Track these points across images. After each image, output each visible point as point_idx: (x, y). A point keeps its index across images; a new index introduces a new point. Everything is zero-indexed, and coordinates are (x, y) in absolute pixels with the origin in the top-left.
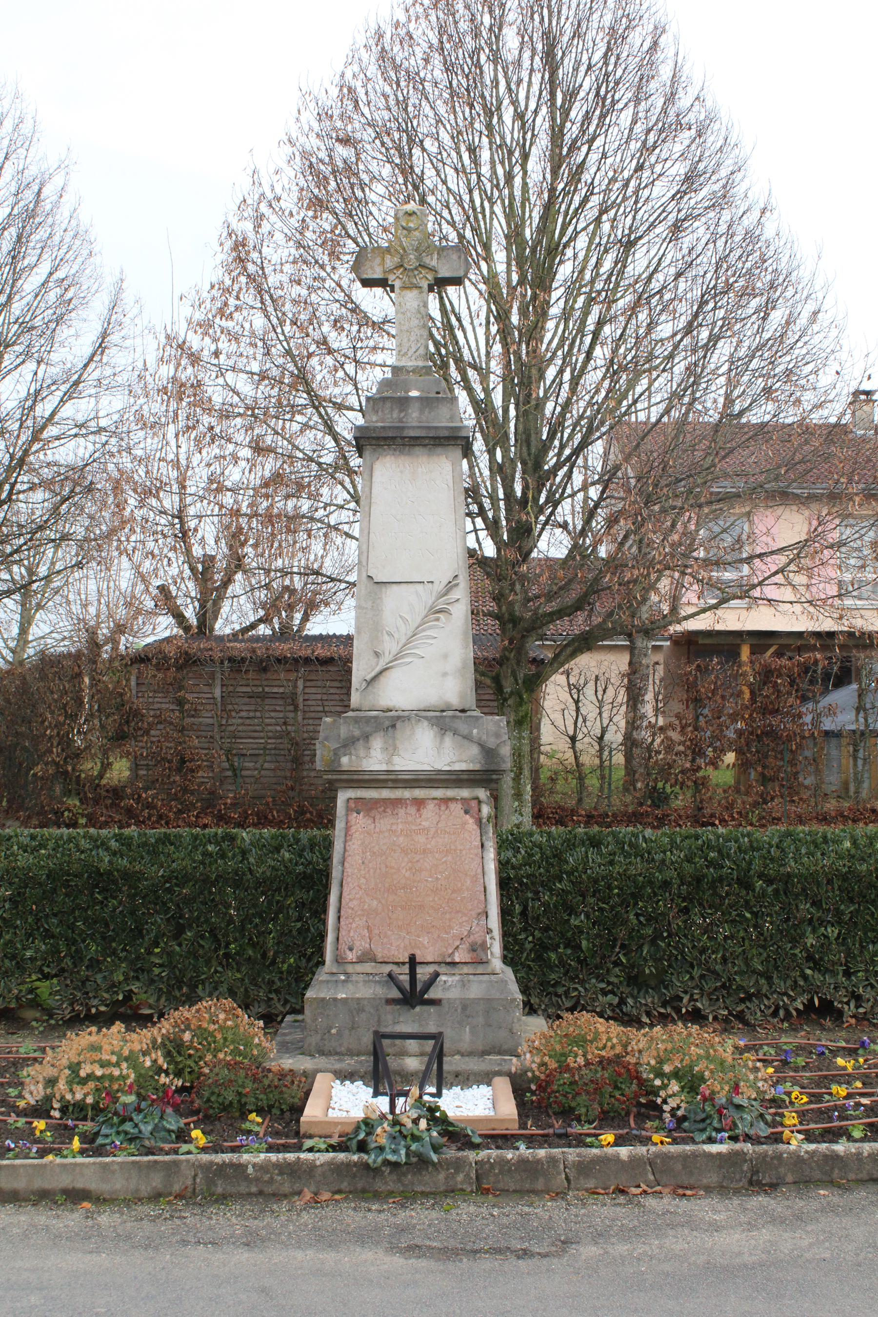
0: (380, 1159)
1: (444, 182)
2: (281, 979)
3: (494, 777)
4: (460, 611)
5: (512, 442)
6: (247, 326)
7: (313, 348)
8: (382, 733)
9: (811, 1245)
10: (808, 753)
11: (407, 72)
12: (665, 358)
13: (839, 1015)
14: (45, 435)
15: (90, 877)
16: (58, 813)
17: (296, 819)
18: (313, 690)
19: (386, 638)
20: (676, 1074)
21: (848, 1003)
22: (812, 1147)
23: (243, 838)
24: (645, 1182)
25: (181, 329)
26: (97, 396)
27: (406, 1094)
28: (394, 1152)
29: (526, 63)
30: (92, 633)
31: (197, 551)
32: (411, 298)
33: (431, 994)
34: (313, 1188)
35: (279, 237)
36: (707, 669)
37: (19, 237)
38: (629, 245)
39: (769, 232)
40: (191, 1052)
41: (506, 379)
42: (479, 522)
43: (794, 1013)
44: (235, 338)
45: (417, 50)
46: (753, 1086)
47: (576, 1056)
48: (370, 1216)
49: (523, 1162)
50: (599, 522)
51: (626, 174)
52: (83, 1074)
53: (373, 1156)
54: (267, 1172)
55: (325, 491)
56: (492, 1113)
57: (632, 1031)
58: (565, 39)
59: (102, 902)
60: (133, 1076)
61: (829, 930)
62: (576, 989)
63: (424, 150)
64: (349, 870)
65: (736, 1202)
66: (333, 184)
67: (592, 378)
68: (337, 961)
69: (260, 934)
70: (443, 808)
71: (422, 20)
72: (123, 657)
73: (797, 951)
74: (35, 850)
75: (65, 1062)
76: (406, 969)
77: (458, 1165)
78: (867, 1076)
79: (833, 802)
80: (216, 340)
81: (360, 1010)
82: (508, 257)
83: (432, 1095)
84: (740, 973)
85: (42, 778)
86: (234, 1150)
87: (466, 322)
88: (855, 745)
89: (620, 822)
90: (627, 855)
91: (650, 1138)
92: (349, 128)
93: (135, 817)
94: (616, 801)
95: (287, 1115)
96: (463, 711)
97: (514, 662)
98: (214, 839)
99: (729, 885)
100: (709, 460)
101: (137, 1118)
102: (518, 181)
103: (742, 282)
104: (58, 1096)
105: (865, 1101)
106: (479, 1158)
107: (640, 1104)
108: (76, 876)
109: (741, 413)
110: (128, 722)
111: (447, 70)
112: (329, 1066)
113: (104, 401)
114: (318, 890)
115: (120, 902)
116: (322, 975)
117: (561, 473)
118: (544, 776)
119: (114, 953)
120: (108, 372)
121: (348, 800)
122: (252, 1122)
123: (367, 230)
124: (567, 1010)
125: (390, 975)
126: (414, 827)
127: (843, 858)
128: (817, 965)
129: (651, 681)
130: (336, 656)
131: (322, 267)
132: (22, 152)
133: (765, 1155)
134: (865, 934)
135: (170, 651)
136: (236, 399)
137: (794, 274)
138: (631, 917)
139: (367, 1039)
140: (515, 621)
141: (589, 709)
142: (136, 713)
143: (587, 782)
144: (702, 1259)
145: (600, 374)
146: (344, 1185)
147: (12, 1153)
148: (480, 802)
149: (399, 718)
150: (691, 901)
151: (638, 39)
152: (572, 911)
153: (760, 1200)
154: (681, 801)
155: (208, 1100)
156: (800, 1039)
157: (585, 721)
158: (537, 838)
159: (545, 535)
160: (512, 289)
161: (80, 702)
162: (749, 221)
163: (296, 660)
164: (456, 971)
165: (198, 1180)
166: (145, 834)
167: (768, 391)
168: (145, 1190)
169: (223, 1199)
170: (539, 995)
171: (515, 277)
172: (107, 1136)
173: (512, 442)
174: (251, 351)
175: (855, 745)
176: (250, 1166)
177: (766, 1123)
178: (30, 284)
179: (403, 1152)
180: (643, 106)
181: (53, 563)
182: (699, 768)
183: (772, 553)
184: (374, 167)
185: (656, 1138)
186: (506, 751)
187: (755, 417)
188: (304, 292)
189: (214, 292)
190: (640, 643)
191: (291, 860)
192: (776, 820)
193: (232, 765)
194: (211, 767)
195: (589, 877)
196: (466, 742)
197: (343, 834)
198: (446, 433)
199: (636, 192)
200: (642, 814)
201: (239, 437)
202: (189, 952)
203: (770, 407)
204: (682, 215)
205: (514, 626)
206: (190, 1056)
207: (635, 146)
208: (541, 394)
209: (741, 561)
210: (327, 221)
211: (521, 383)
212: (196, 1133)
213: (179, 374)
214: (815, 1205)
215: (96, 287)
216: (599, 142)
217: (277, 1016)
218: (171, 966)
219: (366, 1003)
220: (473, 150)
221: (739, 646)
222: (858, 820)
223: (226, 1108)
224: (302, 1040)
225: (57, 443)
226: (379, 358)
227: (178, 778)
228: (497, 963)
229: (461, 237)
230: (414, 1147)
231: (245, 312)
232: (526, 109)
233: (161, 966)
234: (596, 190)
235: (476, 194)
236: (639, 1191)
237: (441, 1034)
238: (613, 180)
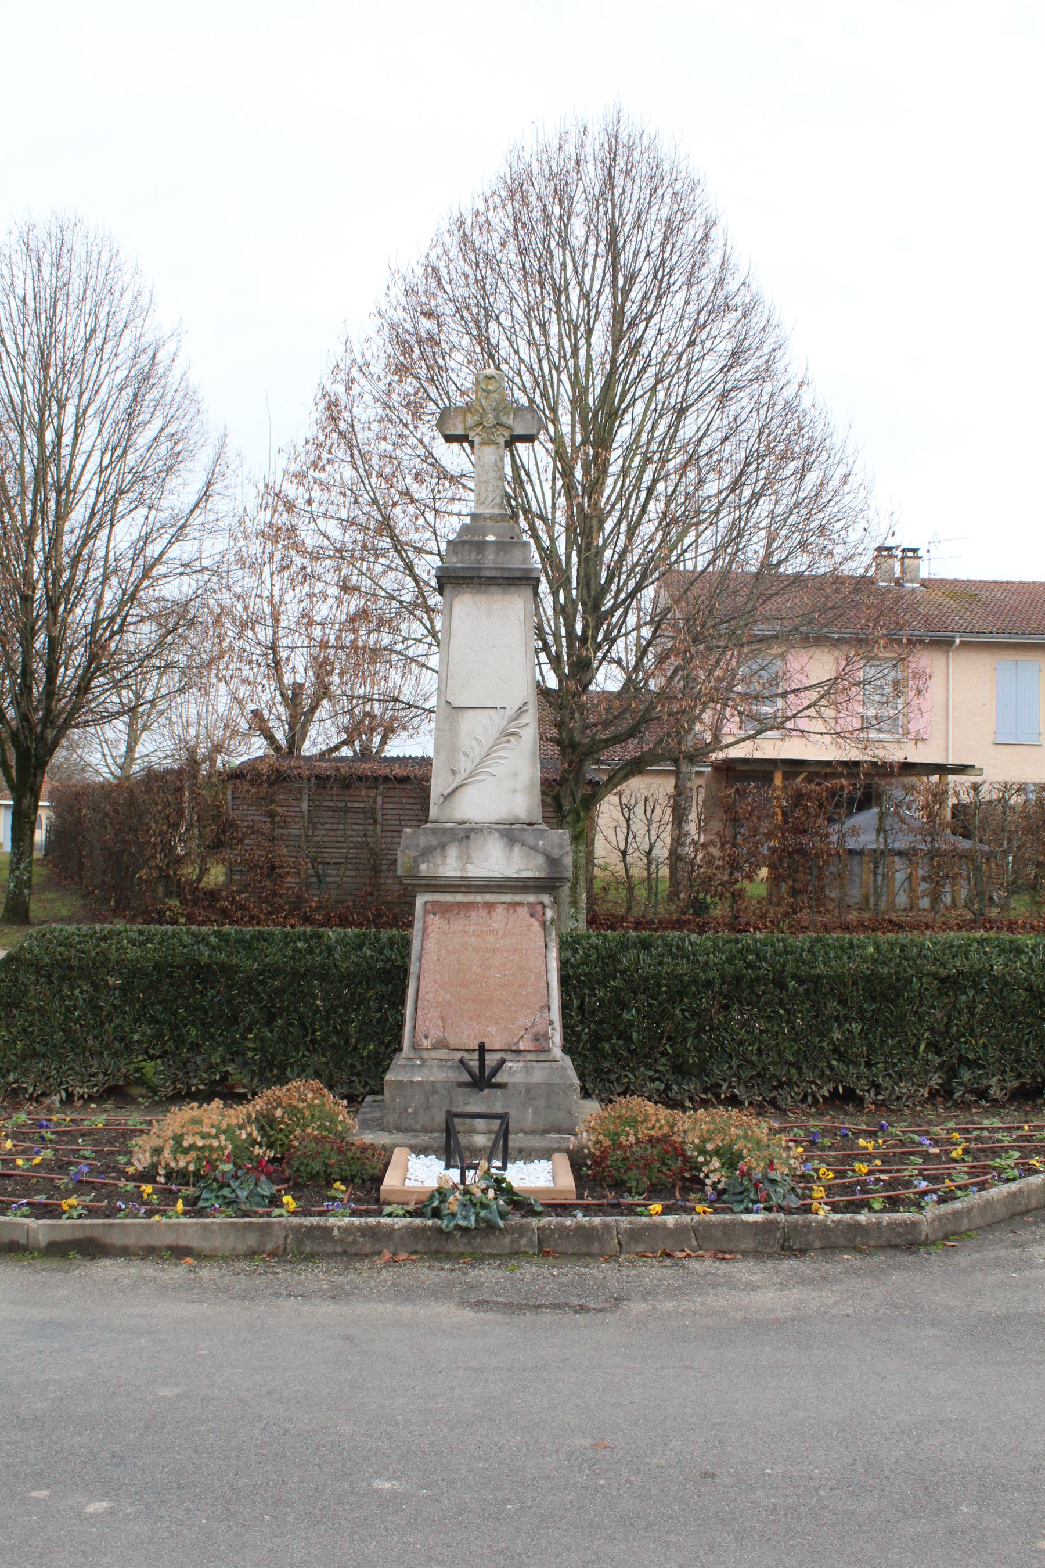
0: (452, 1224)
1: (517, 352)
2: (362, 1063)
4: (529, 734)
5: (574, 584)
6: (338, 477)
7: (396, 498)
9: (836, 1303)
10: (833, 869)
11: (486, 254)
12: (711, 513)
14: (154, 573)
15: (191, 969)
16: (161, 913)
17: (374, 921)
18: (391, 806)
19: (462, 757)
20: (717, 1152)
21: (868, 1091)
22: (838, 1217)
25: (277, 479)
26: (201, 539)
27: (475, 1167)
28: (465, 1218)
29: (592, 249)
30: (192, 752)
31: (288, 679)
32: (489, 453)
33: (499, 1079)
34: (392, 1249)
35: (367, 398)
36: (744, 792)
37: (135, 396)
38: (681, 412)
39: (806, 403)
41: (569, 528)
42: (543, 657)
44: (326, 487)
45: (495, 235)
46: (786, 1163)
47: (628, 1135)
48: (443, 1274)
49: (580, 1229)
50: (649, 660)
51: (680, 348)
52: (185, 1144)
55: (404, 626)
56: (552, 1185)
57: (678, 1113)
58: (627, 228)
63: (500, 324)
64: (425, 966)
65: (770, 1264)
66: (417, 351)
67: (647, 529)
71: (499, 210)
72: (220, 774)
73: (824, 1044)
74: (143, 944)
75: (169, 1133)
77: (522, 1230)
78: (885, 1155)
79: (855, 913)
80: (309, 490)
82: (573, 419)
83: (498, 1168)
85: (146, 881)
86: (321, 1214)
88: (876, 863)
89: (665, 929)
90: (674, 957)
91: (693, 1209)
92: (433, 303)
93: (230, 917)
94: (661, 909)
95: (368, 1184)
96: (530, 824)
97: (573, 783)
98: (300, 937)
99: (766, 985)
100: (750, 605)
101: (234, 1184)
102: (582, 353)
103: (782, 446)
104: (163, 1164)
105: (884, 1177)
106: (541, 1224)
107: (684, 1178)
110: (224, 832)
111: (521, 253)
112: (405, 1141)
113: (207, 544)
115: (219, 993)
116: (399, 1060)
118: (597, 885)
119: (212, 1037)
120: (212, 517)
121: (426, 903)
122: (337, 1190)
123: (447, 394)
124: (619, 1095)
125: (461, 1061)
127: (866, 962)
128: (841, 1056)
129: (694, 803)
130: (412, 775)
131: (406, 426)
133: (796, 1224)
134: (885, 1029)
136: (326, 542)
137: (828, 441)
138: (678, 1012)
139: (440, 1118)
140: (574, 746)
141: (639, 826)
142: (232, 824)
143: (636, 892)
144: (739, 1315)
146: (420, 1247)
147: (122, 1214)
148: (544, 907)
149: (472, 829)
150: (731, 999)
151: (691, 231)
152: (625, 1006)
153: (789, 1264)
154: (719, 911)
155: (298, 1170)
156: (825, 1122)
157: (635, 837)
158: (594, 940)
159: (602, 669)
160: (576, 449)
161: (180, 812)
162: (788, 393)
163: (376, 779)
164: (520, 1058)
167: (803, 545)
168: (241, 1248)
169: (310, 1257)
170: (593, 1081)
171: (579, 438)
172: (207, 1200)
173: (574, 584)
174: (341, 499)
175: (876, 863)
177: (797, 1196)
178: (143, 439)
179: (473, 1218)
180: (694, 289)
181: (158, 689)
182: (737, 881)
183: (805, 689)
184: (454, 338)
185: (699, 1208)
186: (568, 861)
187: (794, 566)
188: (390, 448)
189: (309, 446)
190: (685, 768)
191: (372, 957)
192: (804, 929)
195: (640, 976)
196: (533, 852)
197: (420, 934)
198: (518, 574)
199: (689, 364)
201: (328, 577)
202: (279, 1038)
203: (806, 558)
204: (728, 386)
205: (573, 751)
206: (281, 1130)
208: (600, 543)
209: (777, 695)
210: (410, 385)
211: (581, 534)
212: (287, 1199)
213: (274, 521)
214: (839, 1268)
215: (202, 441)
216: (655, 320)
218: (263, 1050)
220: (543, 326)
221: (772, 773)
222: (877, 929)
223: (314, 1177)
224: (381, 1118)
225: (164, 580)
226: (456, 507)
227: (268, 883)
228: (557, 1052)
229: (531, 401)
230: (482, 1214)
231: (336, 465)
233: (254, 1050)
234: (653, 362)
235: (545, 364)
237: (506, 1114)
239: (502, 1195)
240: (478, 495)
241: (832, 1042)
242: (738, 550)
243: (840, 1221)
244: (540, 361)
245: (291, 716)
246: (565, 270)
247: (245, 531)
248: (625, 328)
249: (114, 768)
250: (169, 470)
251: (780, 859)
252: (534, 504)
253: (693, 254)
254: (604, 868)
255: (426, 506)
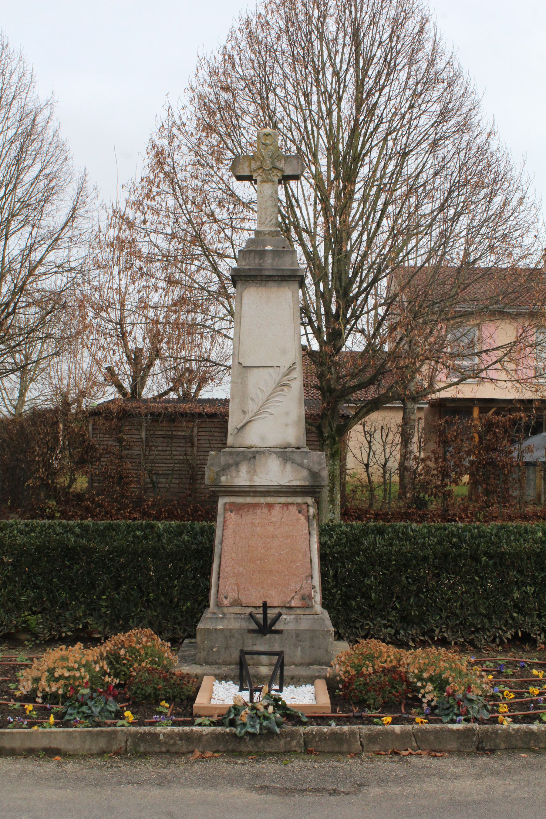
0: (243, 731)
1: (289, 115)
2: (182, 616)
3: (317, 490)
4: (297, 385)
5: (330, 279)
6: (164, 204)
7: (205, 219)
8: (247, 462)
10: (514, 476)
12: (426, 226)
13: (534, 642)
14: (36, 272)
15: (62, 551)
16: (43, 510)
18: (204, 434)
19: (250, 401)
20: (431, 679)
21: (540, 635)
22: (517, 726)
23: (159, 527)
24: (411, 747)
25: (122, 206)
26: (69, 248)
27: (260, 690)
28: (253, 726)
29: (341, 41)
30: (65, 396)
31: (131, 346)
32: (267, 188)
33: (277, 627)
34: (201, 749)
35: (184, 148)
36: (451, 422)
37: (22, 148)
38: (404, 155)
39: (493, 147)
40: (125, 662)
41: (327, 239)
43: (506, 641)
44: (156, 212)
45: (272, 32)
47: (368, 666)
48: (237, 767)
49: (334, 734)
50: (384, 330)
51: (403, 111)
52: (56, 675)
53: (239, 729)
54: (172, 738)
55: (212, 308)
56: (314, 703)
57: (403, 652)
58: (365, 25)
59: (69, 567)
60: (88, 676)
61: (528, 588)
62: (368, 624)
64: (225, 548)
65: (468, 760)
67: (381, 238)
68: (217, 605)
69: (169, 588)
70: (285, 509)
71: (275, 14)
72: (84, 412)
73: (508, 602)
74: (28, 533)
75: (45, 667)
76: (261, 611)
77: (292, 735)
79: (531, 507)
80: (144, 213)
81: (232, 636)
82: (329, 162)
84: (471, 615)
85: (32, 487)
86: (151, 724)
87: (302, 203)
89: (396, 519)
90: (401, 540)
91: (414, 720)
92: (229, 81)
94: (393, 505)
96: (298, 448)
98: (140, 527)
100: (454, 290)
101: (90, 703)
102: (335, 114)
103: (475, 179)
104: (41, 689)
108: (53, 550)
109: (475, 261)
110: (87, 453)
111: (291, 44)
112: (212, 671)
113: (74, 251)
114: (206, 560)
115: (81, 567)
116: (207, 614)
117: (361, 298)
118: (348, 489)
119: (77, 598)
120: (77, 233)
121: (226, 503)
122: (163, 706)
125: (251, 614)
126: (266, 521)
127: (537, 543)
131: (212, 168)
132: (23, 94)
133: (487, 731)
135: (114, 408)
136: (156, 250)
137: (509, 174)
138: (403, 579)
139: (236, 655)
141: (377, 447)
142: (92, 448)
143: (376, 493)
144: (447, 797)
145: (385, 236)
146: (221, 747)
148: (308, 506)
149: (257, 452)
151: (411, 26)
152: (366, 575)
153: (483, 760)
154: (434, 506)
155: (136, 693)
157: (374, 454)
158: (344, 528)
159: (350, 338)
160: (331, 182)
161: (57, 440)
163: (193, 415)
164: (292, 612)
165: (128, 743)
166: (97, 524)
167: (491, 248)
168: (95, 749)
169: (144, 755)
171: (333, 175)
172: (71, 715)
173: (330, 279)
176: (161, 735)
177: (488, 710)
178: (28, 177)
179: (258, 727)
181: (41, 353)
182: (446, 485)
183: (494, 349)
184: (244, 105)
185: (418, 719)
186: (325, 474)
187: (483, 264)
188: (200, 184)
189: (143, 183)
190: (410, 405)
191: (188, 541)
192: (495, 518)
193: (152, 481)
194: (139, 482)
195: (377, 554)
196: (300, 468)
197: (222, 525)
198: (289, 273)
199: (410, 120)
200: (410, 514)
201: (158, 274)
203: (493, 257)
204: (438, 136)
206: (124, 664)
207: (408, 93)
208: (349, 249)
210: (214, 139)
212: (128, 713)
214: (519, 763)
215: (69, 179)
216: (386, 90)
217: (179, 639)
219: (235, 632)
220: (307, 95)
223: (146, 697)
224: (195, 655)
225: (44, 277)
226: (247, 225)
227: (118, 488)
228: (318, 608)
229: (299, 149)
230: (265, 723)
231: (163, 196)
232: (340, 69)
233: (106, 607)
236: (407, 753)
238: (395, 114)
239: (279, 710)
240: (260, 217)
241: (513, 600)
242: (445, 253)
243: (518, 730)
244: (305, 121)
245: (134, 372)
246: (322, 56)
247: (100, 242)
248: (364, 96)
249: (10, 408)
250: (46, 200)
251: (477, 470)
252: (301, 222)
253: (412, 43)
254: (352, 477)
255: (226, 224)
